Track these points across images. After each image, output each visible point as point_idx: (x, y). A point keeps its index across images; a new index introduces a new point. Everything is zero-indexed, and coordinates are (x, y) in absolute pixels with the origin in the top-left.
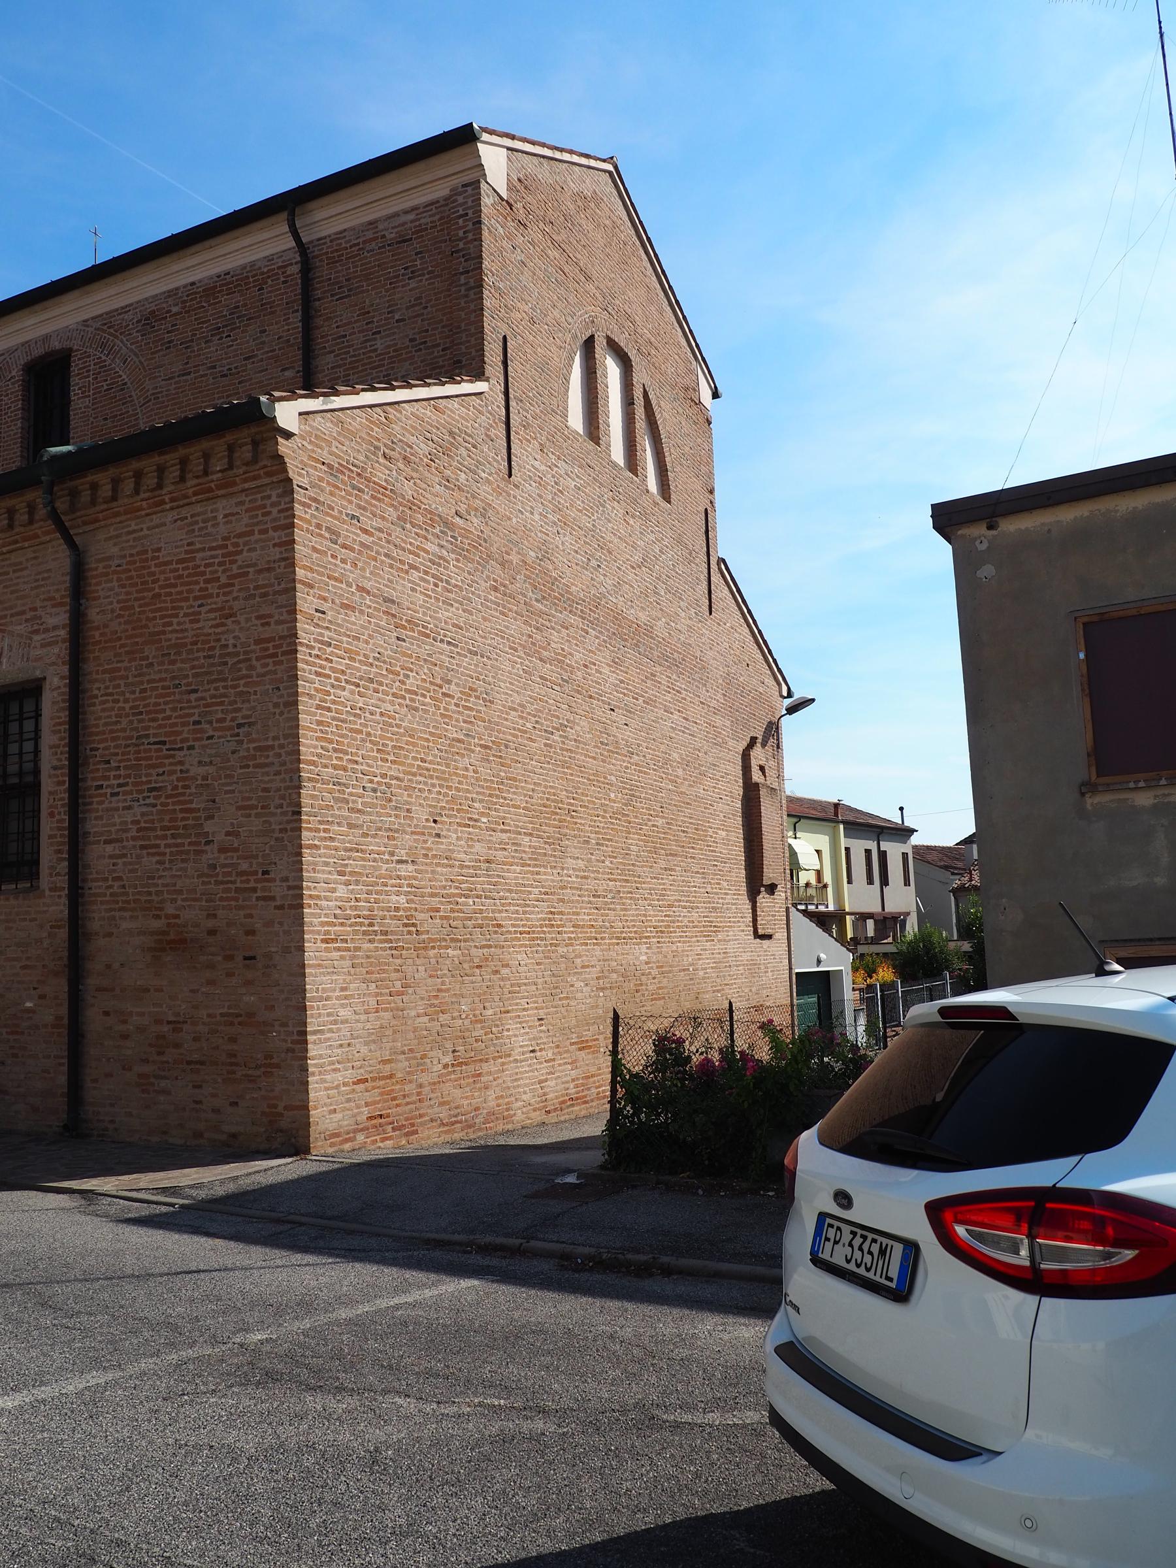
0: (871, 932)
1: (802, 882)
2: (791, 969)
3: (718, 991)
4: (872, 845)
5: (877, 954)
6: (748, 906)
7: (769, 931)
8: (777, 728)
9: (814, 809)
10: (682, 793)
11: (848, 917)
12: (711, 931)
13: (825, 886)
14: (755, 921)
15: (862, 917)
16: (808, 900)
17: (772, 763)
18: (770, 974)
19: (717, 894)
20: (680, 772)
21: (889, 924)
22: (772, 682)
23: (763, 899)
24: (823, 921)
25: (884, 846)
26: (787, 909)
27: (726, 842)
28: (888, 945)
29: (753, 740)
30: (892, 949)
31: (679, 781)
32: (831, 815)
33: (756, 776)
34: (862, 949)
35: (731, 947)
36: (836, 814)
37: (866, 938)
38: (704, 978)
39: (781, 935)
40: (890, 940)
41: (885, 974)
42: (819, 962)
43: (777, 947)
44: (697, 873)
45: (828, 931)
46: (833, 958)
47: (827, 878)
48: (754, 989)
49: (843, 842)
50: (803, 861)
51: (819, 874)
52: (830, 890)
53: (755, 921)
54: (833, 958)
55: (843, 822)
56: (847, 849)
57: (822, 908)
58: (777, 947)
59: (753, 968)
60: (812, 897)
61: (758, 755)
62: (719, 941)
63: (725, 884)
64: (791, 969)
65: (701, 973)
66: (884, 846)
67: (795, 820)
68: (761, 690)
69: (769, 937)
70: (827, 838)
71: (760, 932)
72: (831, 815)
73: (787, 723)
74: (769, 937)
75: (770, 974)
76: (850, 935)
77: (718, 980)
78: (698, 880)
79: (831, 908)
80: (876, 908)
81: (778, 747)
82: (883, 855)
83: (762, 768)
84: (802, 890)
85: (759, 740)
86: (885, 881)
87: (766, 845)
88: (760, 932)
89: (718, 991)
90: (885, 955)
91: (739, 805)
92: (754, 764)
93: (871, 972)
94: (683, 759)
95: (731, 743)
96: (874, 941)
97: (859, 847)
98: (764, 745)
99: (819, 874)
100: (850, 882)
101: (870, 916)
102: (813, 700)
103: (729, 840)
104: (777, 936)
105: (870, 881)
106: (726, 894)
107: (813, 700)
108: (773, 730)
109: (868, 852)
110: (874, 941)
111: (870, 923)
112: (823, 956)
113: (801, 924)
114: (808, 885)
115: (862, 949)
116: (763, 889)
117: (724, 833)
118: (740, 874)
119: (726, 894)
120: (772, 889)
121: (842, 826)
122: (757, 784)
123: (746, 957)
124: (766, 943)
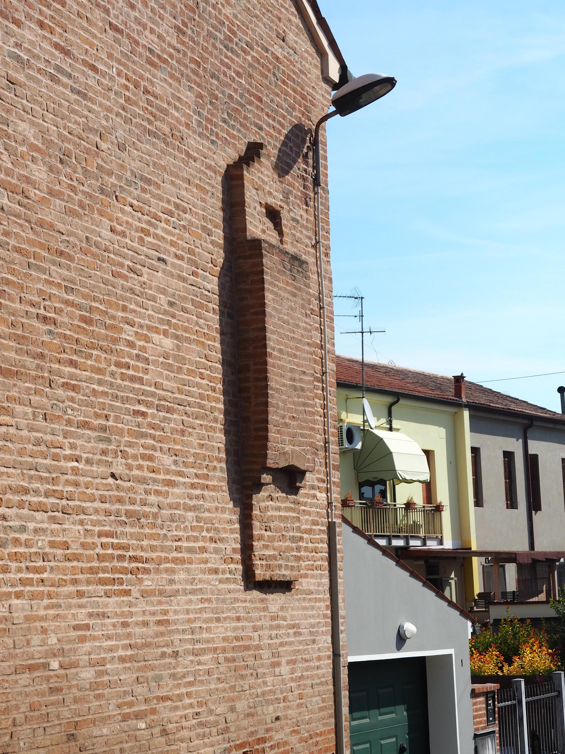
0: (511, 585)
1: (401, 500)
2: (336, 655)
3: (138, 716)
4: (514, 445)
5: (522, 621)
6: (230, 515)
7: (284, 574)
8: (315, 143)
9: (423, 385)
10: (41, 223)
11: (475, 560)
12: (120, 568)
13: (439, 509)
14: (247, 549)
15: (498, 559)
16: (411, 531)
17: (300, 212)
18: (285, 669)
19: (142, 481)
20: (39, 173)
21: (541, 570)
22: (305, 45)
23: (269, 502)
24: (433, 569)
25: (535, 447)
26: (331, 527)
27: (173, 363)
28: (540, 608)
29: (253, 151)
30: (548, 612)
31: (33, 192)
32: (450, 394)
33: (257, 226)
34: (496, 612)
35: (178, 609)
36: (458, 393)
37: (504, 594)
38: (94, 686)
39: (314, 583)
40: (542, 597)
41: (535, 657)
42: (401, 639)
43: (305, 608)
44: (85, 425)
45: (437, 585)
46: (437, 632)
47: (443, 495)
48: (240, 706)
49: (469, 439)
50: (402, 466)
51: (429, 488)
52: (446, 516)
53: (247, 549)
54: (437, 632)
55: (472, 407)
56: (475, 451)
57: (432, 545)
58: (305, 608)
59: (240, 658)
60: (415, 527)
61: (262, 185)
62: (144, 594)
63: (167, 460)
64: (336, 655)
65: (88, 674)
66: (535, 447)
67: (389, 400)
68: (279, 52)
69: (285, 586)
70: (442, 432)
71: (260, 574)
72: (450, 394)
73: (342, 136)
74: (285, 586)
75: (285, 669)
76: (478, 588)
77: (139, 689)
78: (87, 443)
79: (448, 544)
80: (520, 545)
81: (316, 182)
82: (532, 463)
83: (273, 214)
84: (400, 514)
85: (272, 150)
86: (534, 504)
87: (277, 380)
88: (260, 574)
89: (138, 716)
90: (536, 622)
91: (213, 284)
92: (252, 197)
93: (510, 653)
94: (49, 143)
95: (194, 142)
96: (517, 599)
97: (494, 446)
98: (283, 168)
99: (429, 488)
100: (479, 503)
101: (511, 557)
102: (390, 83)
103: (183, 360)
104: (304, 584)
105: (512, 503)
106: (170, 483)
107: (390, 83)
108: (302, 147)
109: (509, 456)
110: (517, 599)
111: (511, 570)
112: (410, 628)
113: (361, 559)
114: (409, 506)
115: (496, 612)
116: (266, 478)
117: (168, 343)
118: (211, 439)
119: (170, 483)
120: (290, 479)
121: (466, 414)
122: (257, 243)
123: (220, 631)
124: (276, 600)
